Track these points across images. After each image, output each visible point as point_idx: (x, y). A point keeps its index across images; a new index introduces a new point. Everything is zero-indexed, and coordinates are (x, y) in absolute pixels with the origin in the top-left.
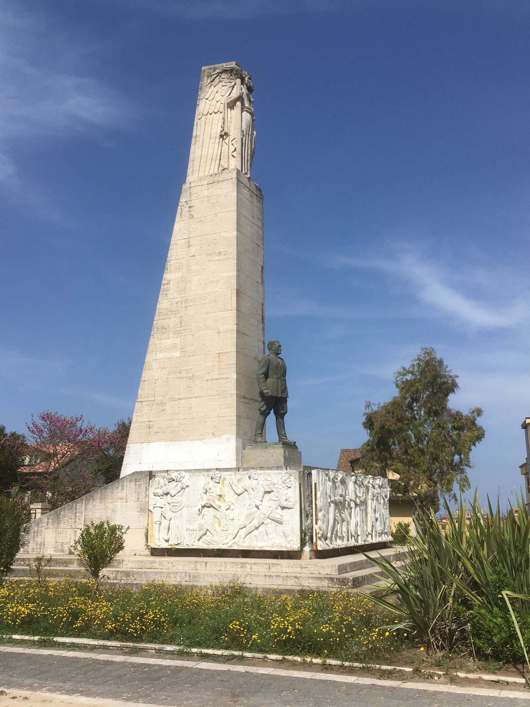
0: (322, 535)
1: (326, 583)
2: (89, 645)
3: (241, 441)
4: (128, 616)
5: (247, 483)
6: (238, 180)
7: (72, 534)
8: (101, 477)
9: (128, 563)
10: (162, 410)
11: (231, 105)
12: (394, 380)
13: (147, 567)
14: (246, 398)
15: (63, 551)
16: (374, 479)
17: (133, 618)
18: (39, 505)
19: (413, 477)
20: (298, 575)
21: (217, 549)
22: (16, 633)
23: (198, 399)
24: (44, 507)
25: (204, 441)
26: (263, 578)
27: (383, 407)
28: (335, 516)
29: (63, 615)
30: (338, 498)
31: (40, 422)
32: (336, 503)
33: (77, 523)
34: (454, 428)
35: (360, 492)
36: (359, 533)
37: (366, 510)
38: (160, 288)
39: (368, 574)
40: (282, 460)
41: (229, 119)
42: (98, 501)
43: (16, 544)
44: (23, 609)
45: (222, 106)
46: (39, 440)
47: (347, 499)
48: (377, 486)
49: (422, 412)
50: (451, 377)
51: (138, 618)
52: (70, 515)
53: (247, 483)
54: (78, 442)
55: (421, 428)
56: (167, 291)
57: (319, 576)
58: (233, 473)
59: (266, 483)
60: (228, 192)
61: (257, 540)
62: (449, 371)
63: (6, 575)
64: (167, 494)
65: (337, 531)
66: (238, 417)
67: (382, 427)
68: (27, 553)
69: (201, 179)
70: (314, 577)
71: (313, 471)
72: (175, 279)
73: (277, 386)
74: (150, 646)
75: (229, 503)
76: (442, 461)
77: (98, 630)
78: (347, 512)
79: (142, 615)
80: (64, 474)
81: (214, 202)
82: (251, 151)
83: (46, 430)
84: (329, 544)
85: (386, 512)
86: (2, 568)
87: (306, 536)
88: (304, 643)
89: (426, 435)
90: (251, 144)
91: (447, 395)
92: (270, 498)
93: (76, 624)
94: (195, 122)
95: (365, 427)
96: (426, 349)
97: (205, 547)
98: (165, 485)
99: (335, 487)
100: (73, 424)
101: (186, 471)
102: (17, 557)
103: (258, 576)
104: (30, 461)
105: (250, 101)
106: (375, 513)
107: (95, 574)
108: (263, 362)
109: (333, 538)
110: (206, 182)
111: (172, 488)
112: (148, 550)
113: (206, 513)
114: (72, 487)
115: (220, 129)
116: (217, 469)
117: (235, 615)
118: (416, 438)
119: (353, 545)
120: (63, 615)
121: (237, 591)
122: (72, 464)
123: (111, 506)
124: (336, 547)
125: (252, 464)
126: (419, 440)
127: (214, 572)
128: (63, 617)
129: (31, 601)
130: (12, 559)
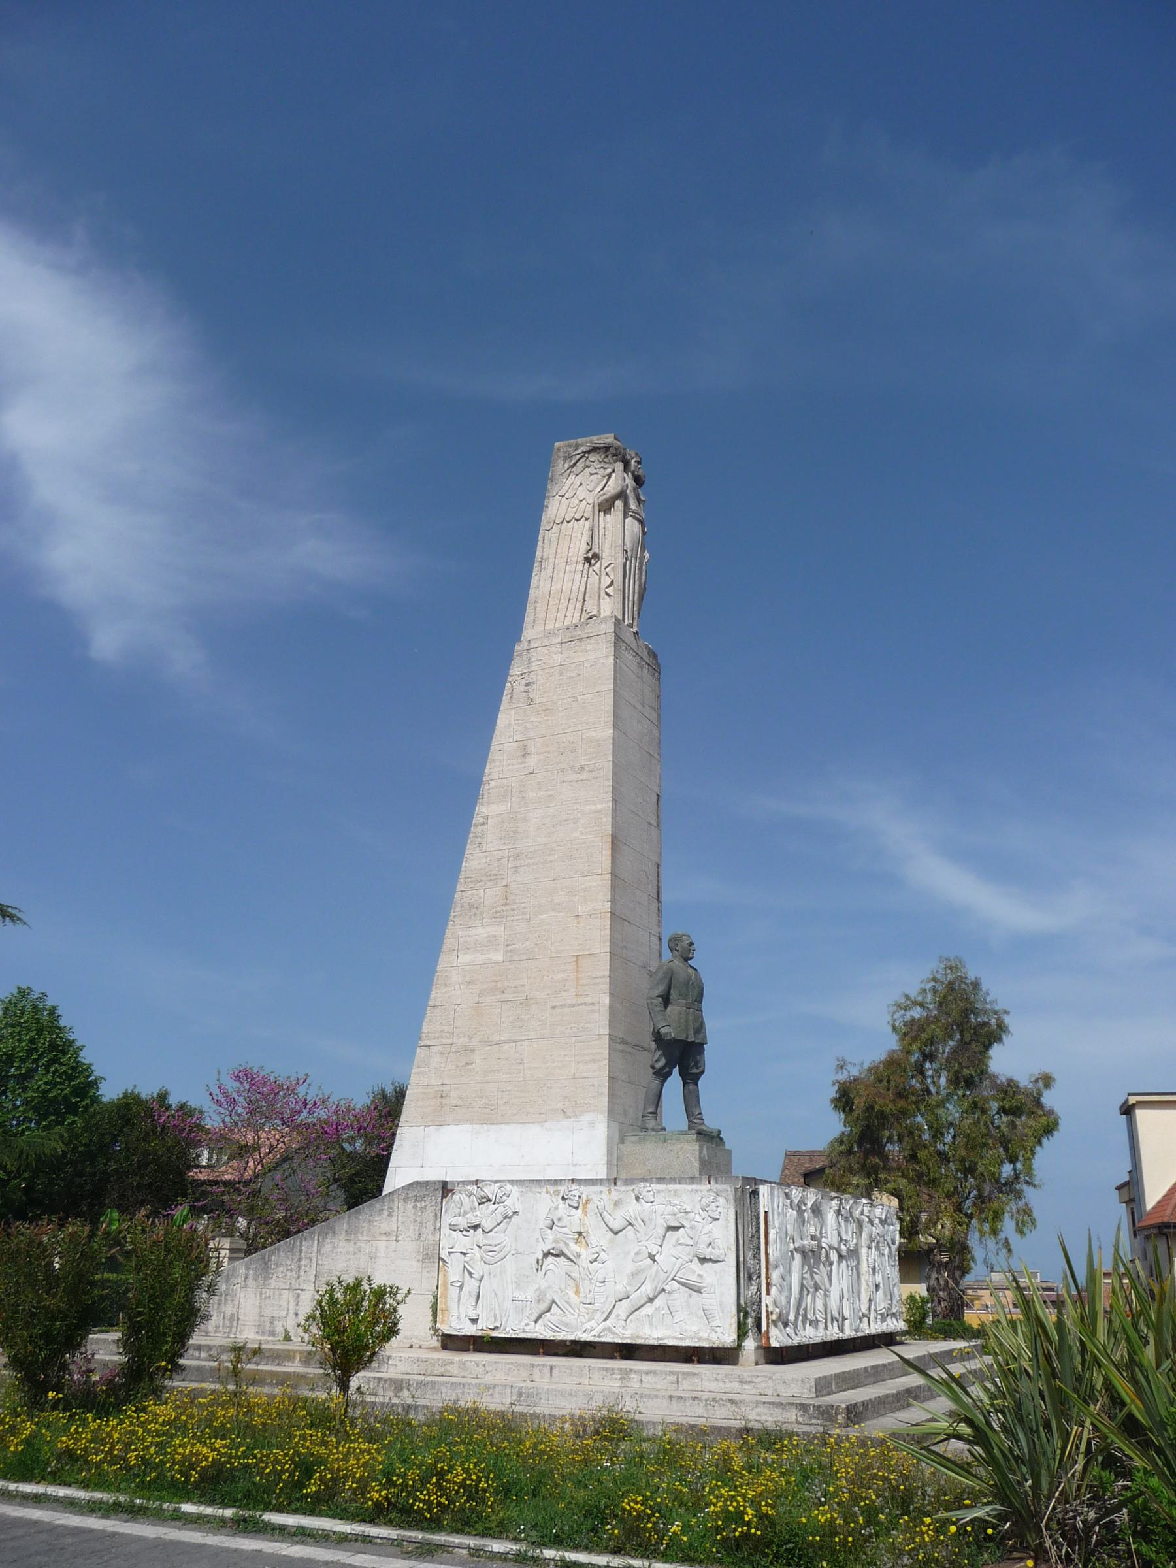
0: (780, 1316)
1: (792, 1415)
2: (334, 1532)
3: (615, 1126)
4: (413, 1474)
5: (632, 1209)
6: (617, 637)
7: (292, 1300)
8: (339, 1192)
9: (398, 1363)
10: (467, 1064)
11: (606, 507)
12: (889, 1018)
13: (435, 1372)
14: (627, 1043)
15: (272, 1333)
16: (872, 1206)
17: (424, 1481)
18: (226, 1243)
19: (925, 1206)
20: (736, 1398)
21: (572, 1342)
22: (189, 1500)
23: (535, 1044)
24: (234, 1246)
25: (547, 1125)
26: (666, 1402)
27: (869, 1070)
28: (803, 1278)
29: (283, 1467)
30: (807, 1242)
31: (231, 1085)
32: (804, 1253)
33: (302, 1278)
34: (1003, 1111)
35: (847, 1232)
36: (846, 1314)
37: (857, 1267)
38: (469, 832)
39: (873, 1397)
40: (697, 1165)
41: (602, 531)
42: (342, 1237)
43: (189, 1317)
44: (205, 1451)
45: (589, 508)
46: (228, 1119)
47: (824, 1245)
48: (877, 1221)
49: (943, 1081)
50: (996, 1013)
51: (434, 1480)
52: (289, 1263)
53: (632, 1209)
54: (300, 1125)
55: (940, 1111)
56: (482, 837)
57: (777, 1400)
58: (604, 1189)
59: (670, 1209)
60: (598, 658)
61: (651, 1324)
62: (992, 1002)
63: (171, 1378)
64: (476, 1227)
65: (805, 1310)
66: (612, 1079)
67: (870, 1108)
68: (211, 1336)
69: (549, 634)
70: (769, 1403)
71: (761, 1187)
72: (497, 816)
73: (687, 1021)
74: (457, 1541)
75: (597, 1249)
76: (982, 1174)
77: (351, 1501)
78: (823, 1270)
79: (441, 1474)
80: (271, 1184)
81: (573, 675)
82: (640, 586)
83: (241, 1099)
84: (793, 1335)
85: (894, 1273)
86: (164, 1363)
87: (748, 1318)
88: (779, 1546)
89: (951, 1124)
90: (640, 573)
91: (987, 1047)
92: (678, 1240)
93: (306, 1488)
94: (540, 536)
95: (836, 1107)
96: (948, 960)
97: (548, 1335)
98: (473, 1209)
99: (801, 1221)
100: (291, 1091)
101: (512, 1182)
102: (191, 1342)
103: (658, 1399)
104: (210, 1159)
105: (639, 500)
106: (874, 1273)
107: (344, 1385)
108: (660, 974)
109: (800, 1323)
110: (559, 640)
111: (486, 1215)
112: (435, 1338)
113: (551, 1267)
114: (286, 1210)
115: (584, 547)
116: (573, 1180)
117: (628, 1482)
118: (932, 1130)
119: (835, 1337)
120: (283, 1467)
121: (614, 1429)
122: (286, 1166)
123: (367, 1248)
124: (805, 1341)
125: (638, 1172)
126: (937, 1134)
127: (568, 1388)
128: (283, 1471)
129: (221, 1433)
130: (183, 1345)
